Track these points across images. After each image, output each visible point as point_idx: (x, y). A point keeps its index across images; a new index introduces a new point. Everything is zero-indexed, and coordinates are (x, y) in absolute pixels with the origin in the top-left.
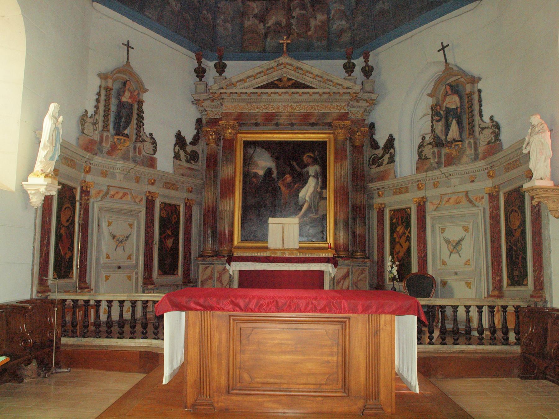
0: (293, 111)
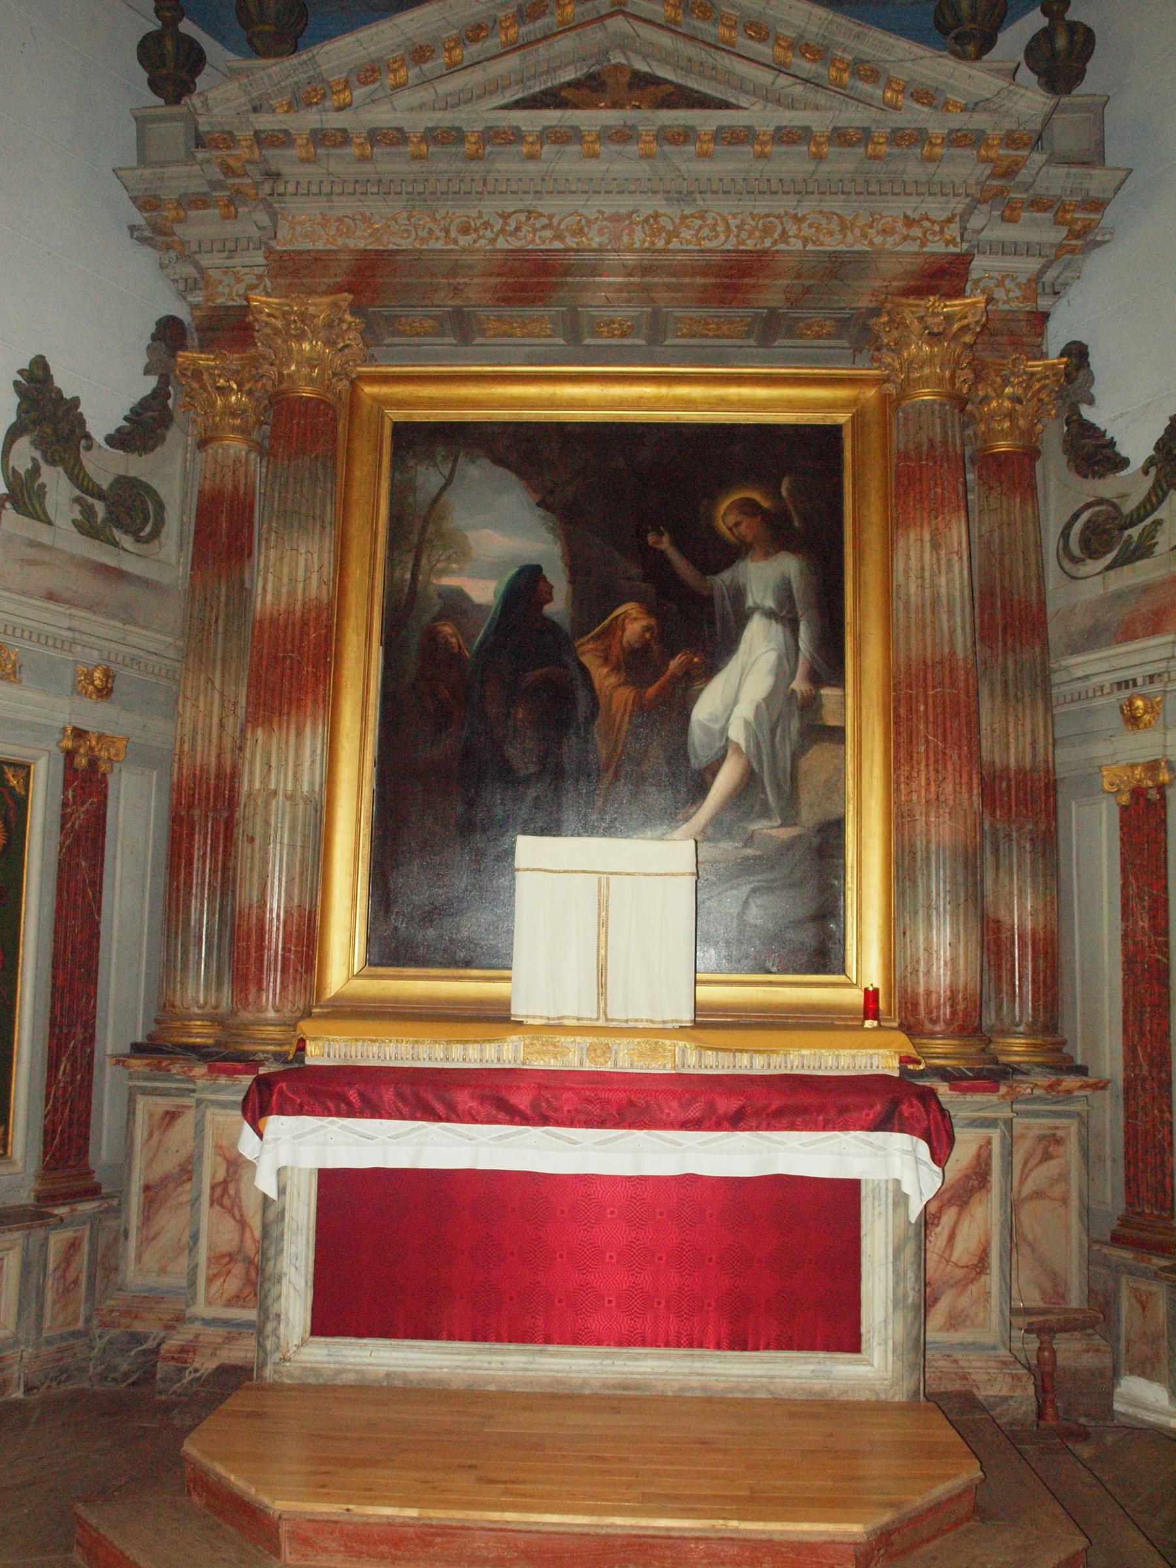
0: (660, 244)
